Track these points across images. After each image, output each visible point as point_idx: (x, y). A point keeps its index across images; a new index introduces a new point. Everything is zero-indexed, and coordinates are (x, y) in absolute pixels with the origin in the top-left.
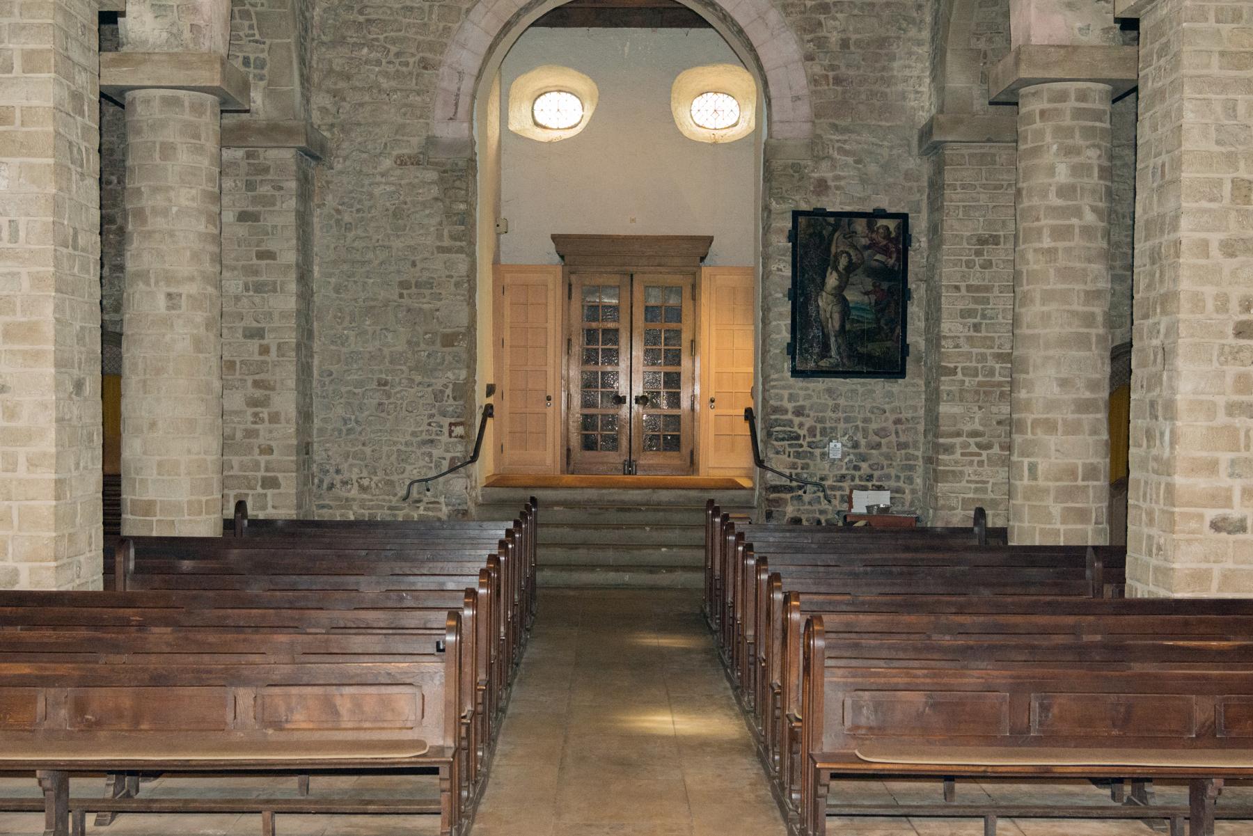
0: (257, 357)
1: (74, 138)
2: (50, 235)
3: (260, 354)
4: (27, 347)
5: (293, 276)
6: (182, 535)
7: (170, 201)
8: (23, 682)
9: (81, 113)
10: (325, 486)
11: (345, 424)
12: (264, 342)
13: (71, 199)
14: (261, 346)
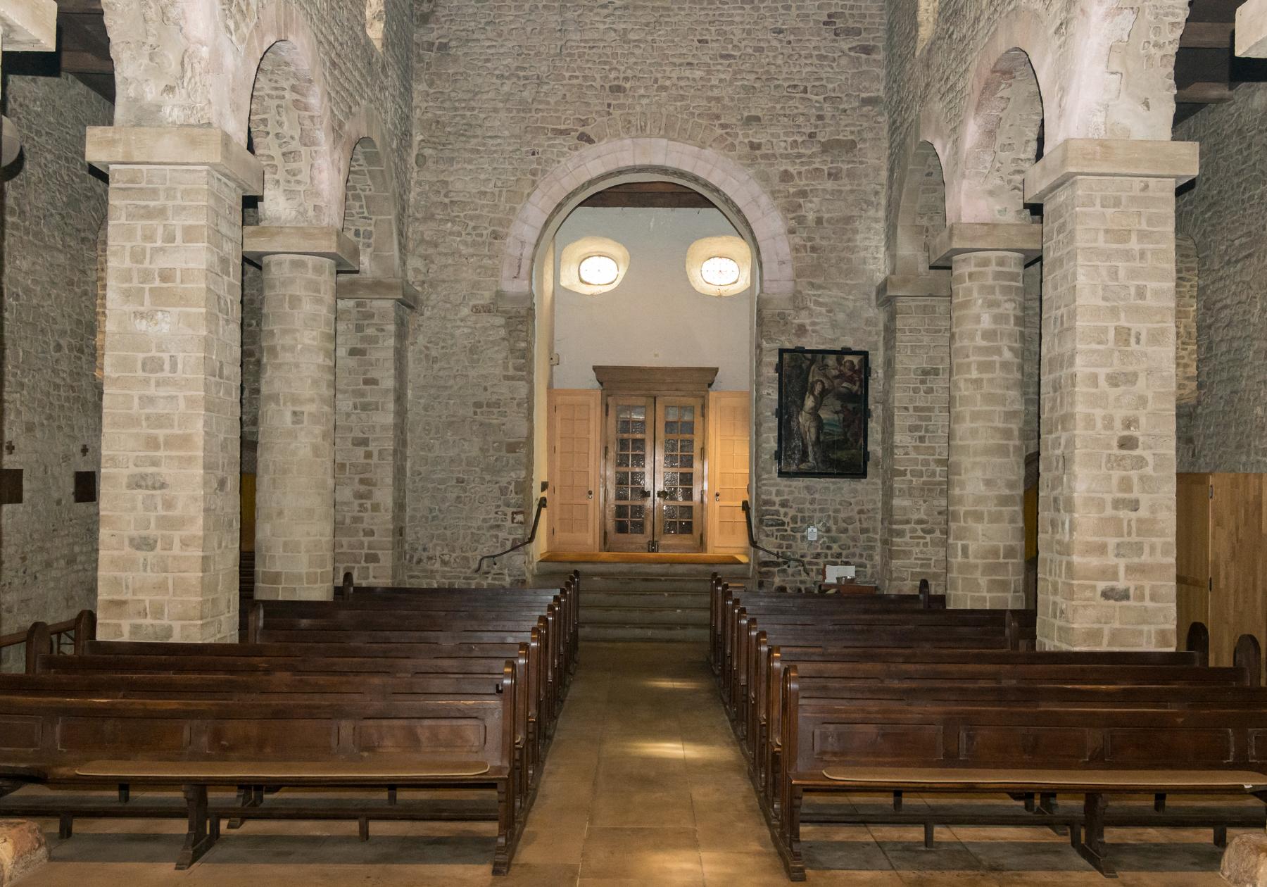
0: (362, 461)
2: (202, 367)
8: (174, 715)
12: (370, 448)
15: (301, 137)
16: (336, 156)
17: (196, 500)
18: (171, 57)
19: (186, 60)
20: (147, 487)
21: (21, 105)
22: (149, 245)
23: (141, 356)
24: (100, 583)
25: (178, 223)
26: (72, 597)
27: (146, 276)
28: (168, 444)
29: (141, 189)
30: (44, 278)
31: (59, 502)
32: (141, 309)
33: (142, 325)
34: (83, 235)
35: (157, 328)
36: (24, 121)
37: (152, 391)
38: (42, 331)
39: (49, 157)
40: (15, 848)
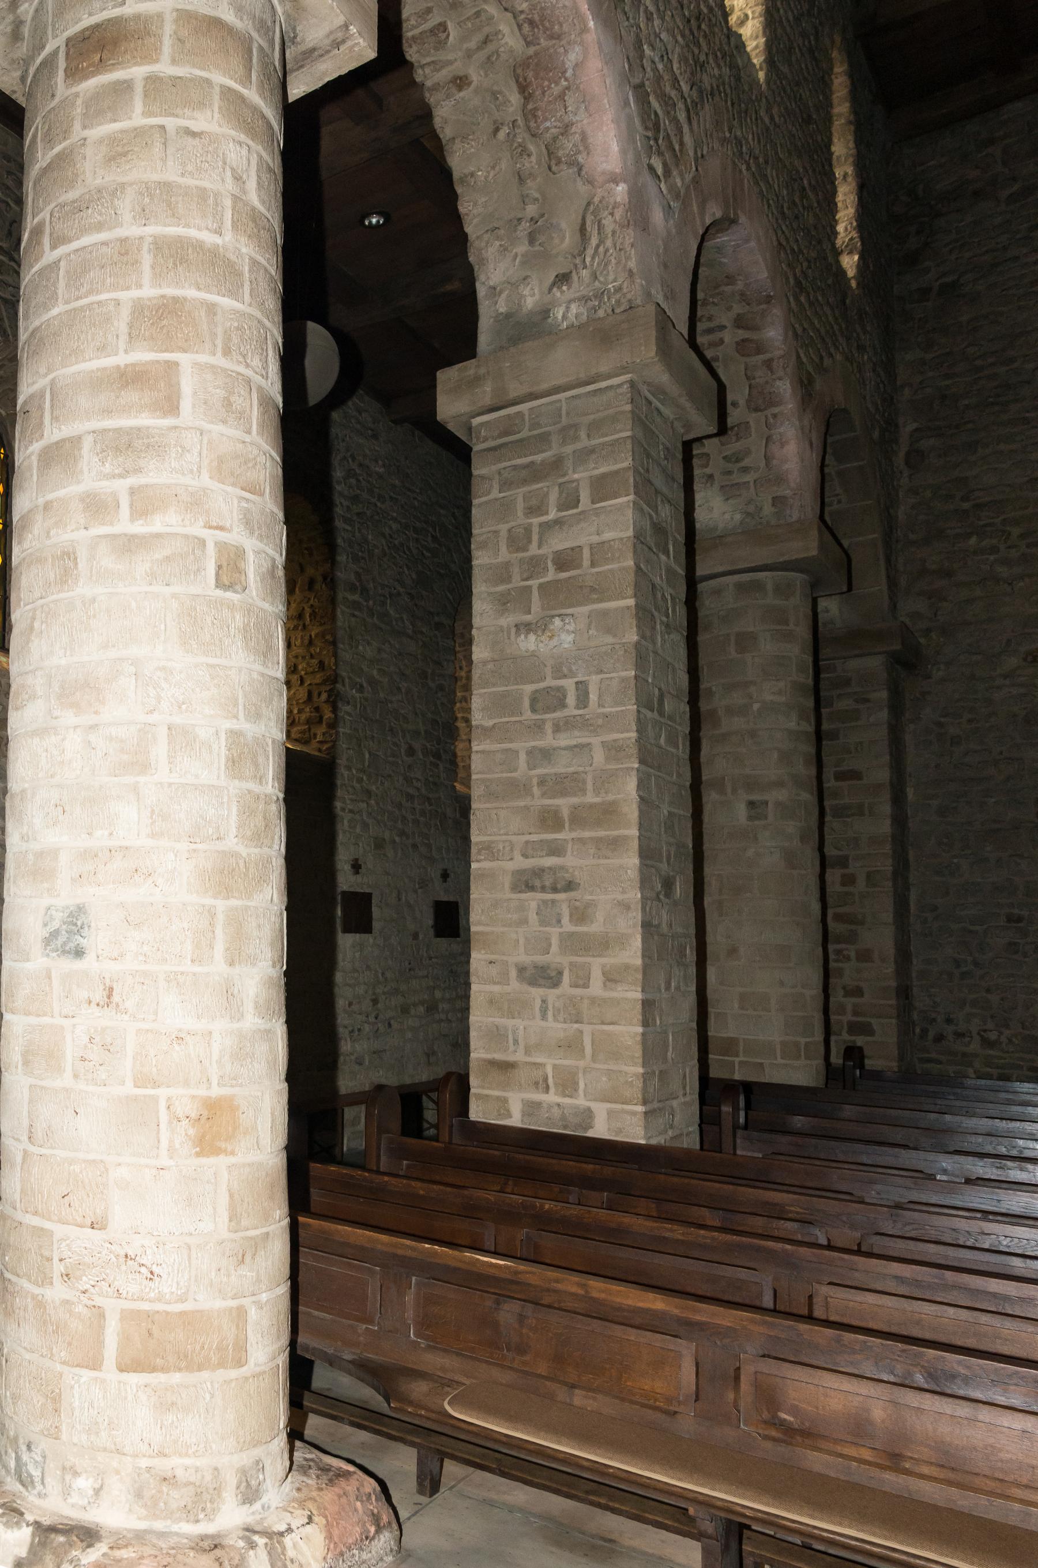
1: (657, 580)
2: (631, 693)
3: (843, 884)
4: (601, 833)
5: (886, 796)
6: (774, 1081)
7: (751, 698)
8: (653, 1323)
9: (667, 553)
10: (931, 1034)
11: (958, 966)
12: (850, 870)
13: (655, 653)
14: (843, 876)
15: (748, 401)
16: (806, 422)
17: (628, 908)
18: (564, 225)
19: (589, 218)
20: (543, 889)
21: (360, 465)
22: (536, 521)
23: (529, 688)
24: (473, 1034)
25: (581, 476)
26: (434, 1053)
27: (534, 566)
28: (578, 819)
29: (521, 440)
30: (392, 668)
31: (415, 936)
32: (528, 618)
33: (529, 643)
34: (436, 619)
35: (555, 642)
36: (364, 483)
37: (548, 740)
38: (391, 730)
39: (395, 526)
40: (329, 1537)
